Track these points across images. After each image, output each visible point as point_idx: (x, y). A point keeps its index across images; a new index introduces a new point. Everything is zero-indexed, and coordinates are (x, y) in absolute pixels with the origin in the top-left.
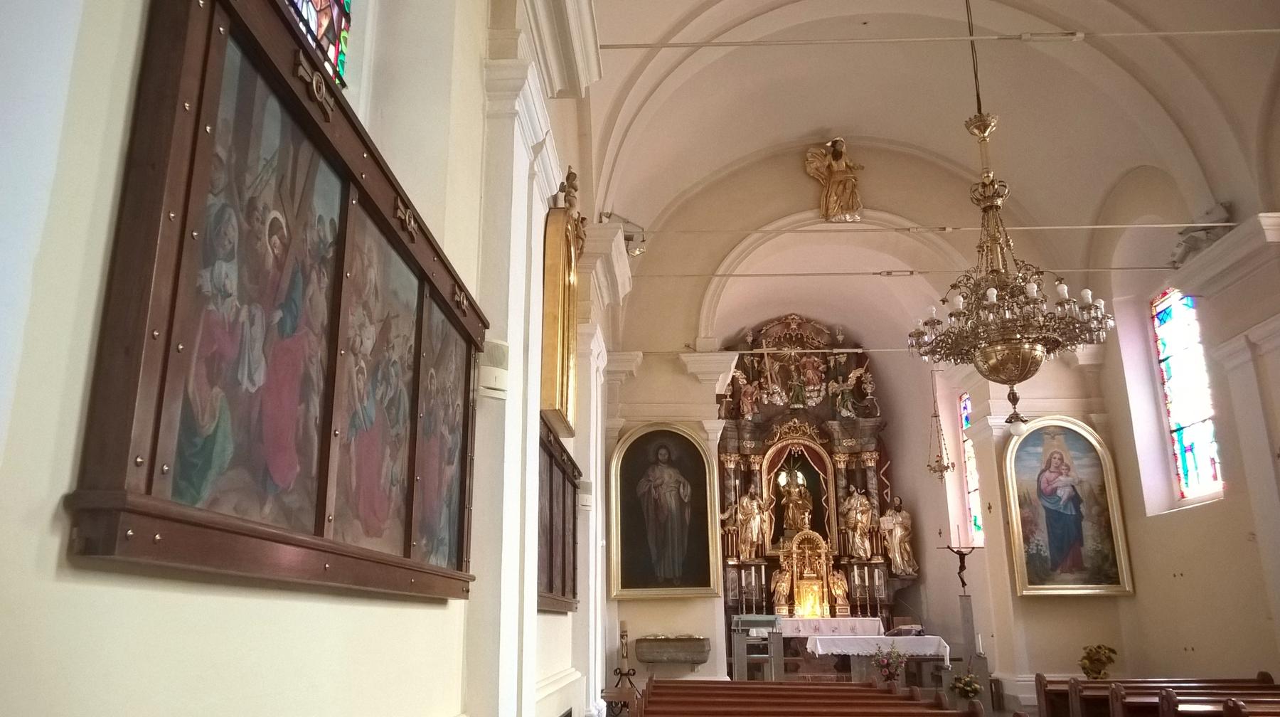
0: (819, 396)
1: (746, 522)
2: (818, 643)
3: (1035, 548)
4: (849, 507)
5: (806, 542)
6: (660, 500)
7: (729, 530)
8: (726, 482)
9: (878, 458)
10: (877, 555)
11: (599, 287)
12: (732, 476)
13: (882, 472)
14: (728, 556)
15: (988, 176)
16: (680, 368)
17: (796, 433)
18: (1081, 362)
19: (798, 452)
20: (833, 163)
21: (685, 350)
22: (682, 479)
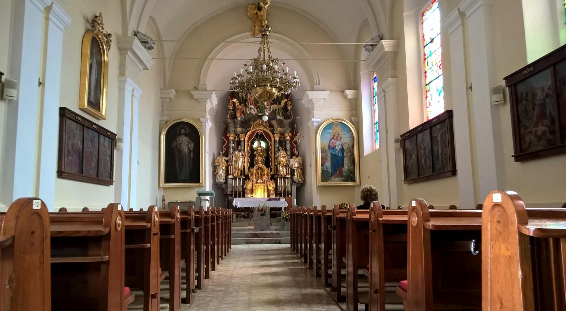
0: (270, 110)
1: (237, 161)
2: (238, 203)
3: (325, 168)
4: (278, 155)
5: (260, 169)
6: (181, 149)
7: (229, 164)
8: (229, 145)
10: (288, 174)
11: (133, 61)
12: (232, 143)
13: (293, 141)
14: (229, 174)
15: (265, 23)
17: (260, 125)
18: (349, 97)
19: (260, 133)
20: (258, 12)
21: (193, 89)
22: (190, 141)
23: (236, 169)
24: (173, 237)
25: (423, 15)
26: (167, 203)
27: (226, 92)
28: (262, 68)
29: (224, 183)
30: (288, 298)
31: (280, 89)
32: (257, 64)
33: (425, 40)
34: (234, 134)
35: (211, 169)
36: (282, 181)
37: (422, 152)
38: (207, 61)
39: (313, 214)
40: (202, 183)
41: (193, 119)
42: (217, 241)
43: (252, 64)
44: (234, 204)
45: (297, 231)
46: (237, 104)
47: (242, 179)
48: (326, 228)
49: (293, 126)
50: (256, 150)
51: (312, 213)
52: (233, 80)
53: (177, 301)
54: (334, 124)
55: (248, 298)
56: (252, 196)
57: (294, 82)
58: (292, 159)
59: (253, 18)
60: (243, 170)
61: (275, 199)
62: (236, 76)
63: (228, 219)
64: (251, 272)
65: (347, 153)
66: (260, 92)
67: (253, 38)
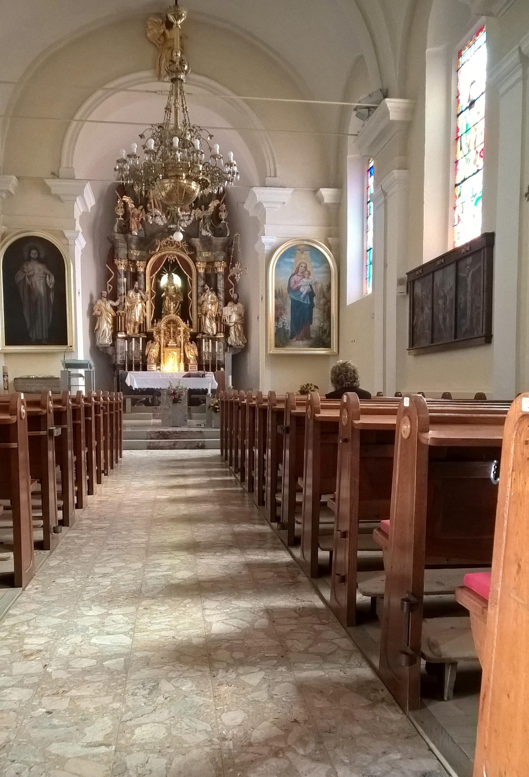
1: (132, 308)
5: (172, 322)
7: (119, 313)
8: (118, 279)
9: (226, 266)
10: (220, 332)
12: (123, 275)
13: (229, 276)
14: (119, 331)
15: (177, 55)
16: (47, 190)
17: (172, 246)
19: (172, 260)
20: (167, 31)
21: (52, 176)
22: (48, 272)
23: (130, 322)
24: (14, 445)
25: (460, 55)
26: (11, 379)
27: (109, 183)
28: (172, 144)
29: (111, 345)
30: (210, 540)
31: (204, 185)
32: (163, 136)
33: (461, 101)
34: (126, 260)
35: (88, 321)
36: (209, 344)
37: (441, 302)
38: (74, 123)
39: (255, 405)
40: (71, 346)
41: (52, 232)
42: (96, 446)
43: (154, 134)
44: (128, 382)
45: (231, 429)
46: (131, 205)
47: (141, 339)
48: (274, 427)
49: (230, 249)
50: (165, 289)
51: (254, 403)
52: (120, 164)
53: (26, 545)
54: (299, 248)
55: (147, 540)
56: (159, 369)
57: (229, 172)
58: (226, 308)
59: (157, 42)
60: (143, 324)
61: (198, 376)
62: (124, 156)
63: (117, 409)
64: (153, 497)
65: (319, 300)
66: (168, 188)
67: (156, 83)
